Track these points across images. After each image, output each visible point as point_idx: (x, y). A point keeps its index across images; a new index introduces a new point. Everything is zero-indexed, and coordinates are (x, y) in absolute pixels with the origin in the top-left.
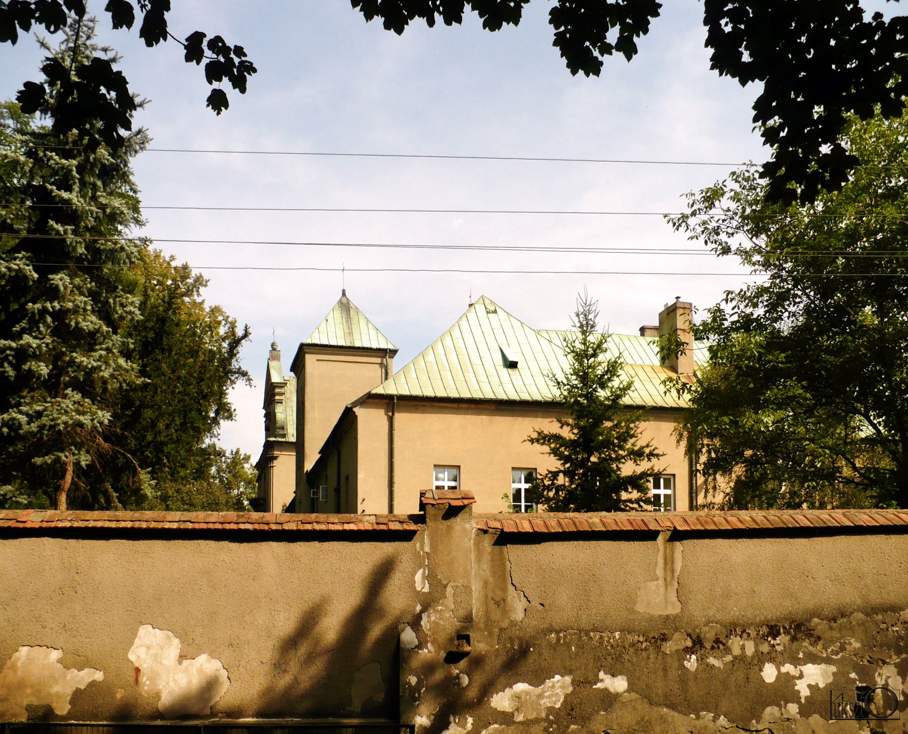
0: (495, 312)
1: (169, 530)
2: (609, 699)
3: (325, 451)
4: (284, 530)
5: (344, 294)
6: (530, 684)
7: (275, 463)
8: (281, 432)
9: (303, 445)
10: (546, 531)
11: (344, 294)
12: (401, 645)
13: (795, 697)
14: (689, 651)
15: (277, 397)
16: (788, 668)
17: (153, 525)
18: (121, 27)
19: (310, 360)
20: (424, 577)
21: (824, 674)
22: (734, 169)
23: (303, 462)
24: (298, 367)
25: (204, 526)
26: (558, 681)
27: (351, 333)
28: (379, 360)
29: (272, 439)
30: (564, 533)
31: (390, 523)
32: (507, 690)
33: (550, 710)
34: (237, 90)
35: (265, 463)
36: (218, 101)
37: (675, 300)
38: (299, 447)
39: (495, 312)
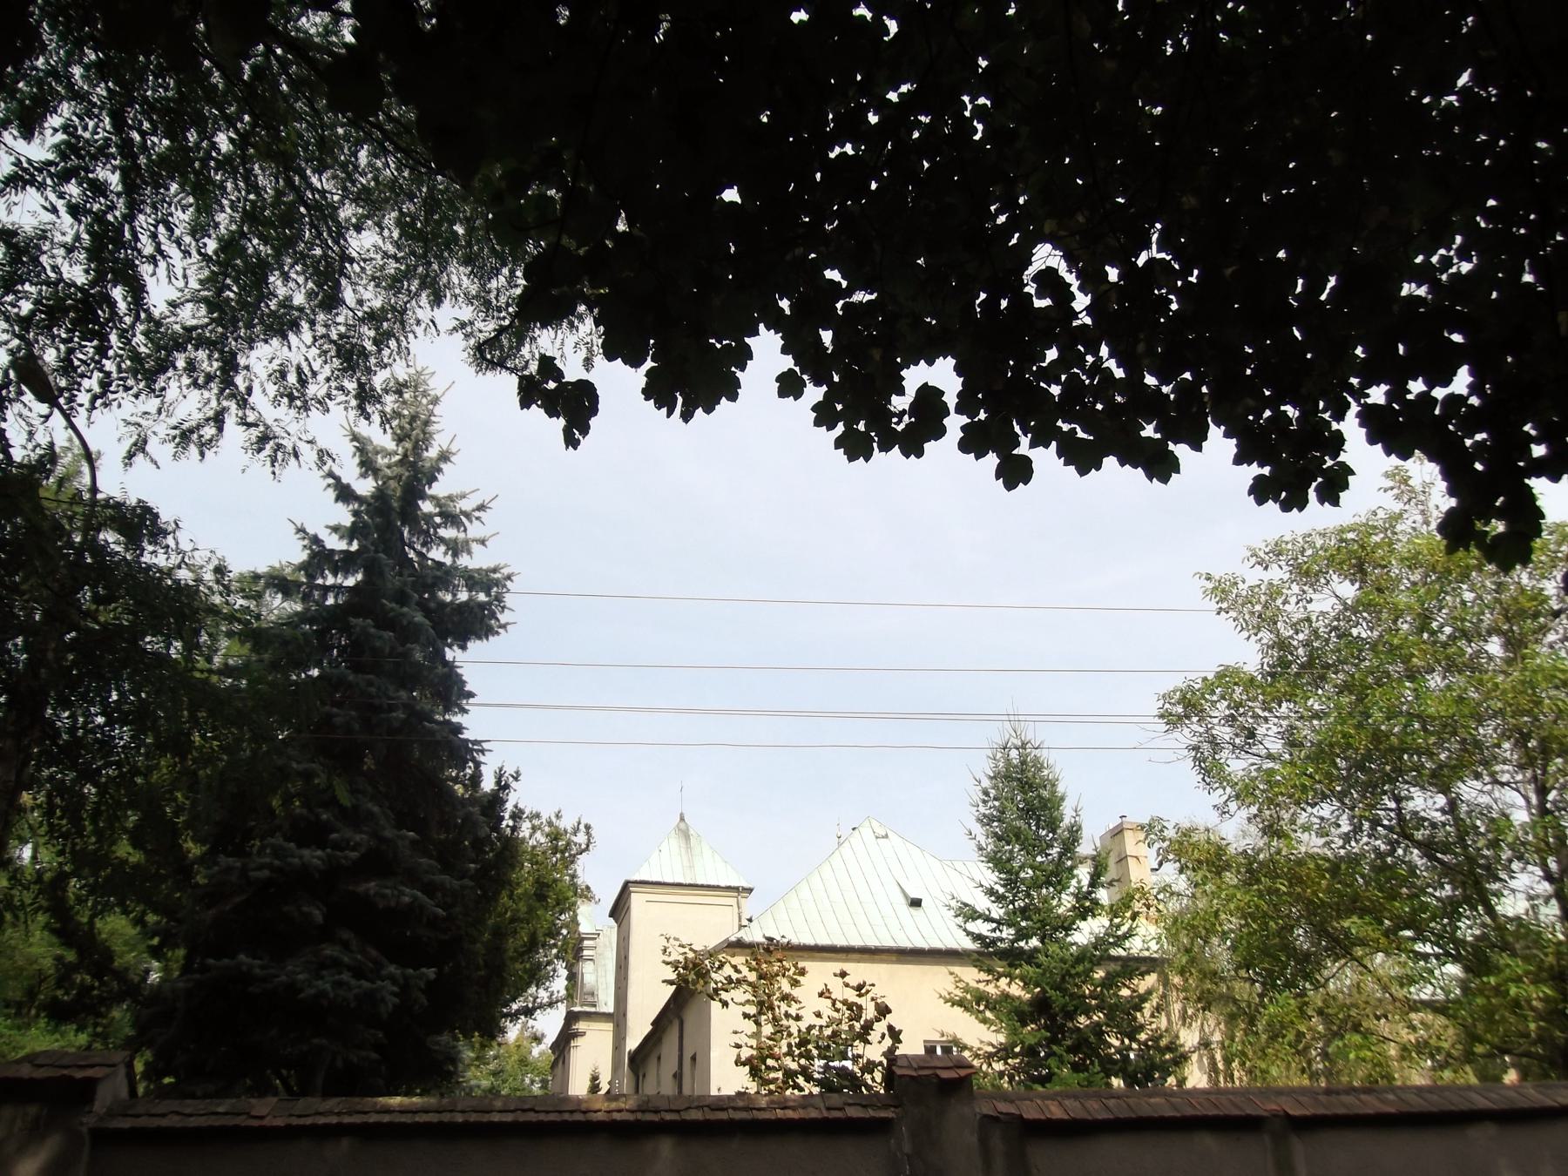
0: (886, 836)
1: (500, 1125)
3: (660, 1023)
4: (684, 1122)
5: (682, 819)
7: (579, 1041)
9: (625, 1015)
10: (1066, 1117)
11: (682, 819)
17: (473, 1118)
19: (637, 900)
22: (1203, 675)
23: (624, 1039)
24: (620, 910)
25: (552, 1117)
27: (691, 867)
28: (733, 901)
31: (847, 1108)
37: (1120, 821)
38: (618, 1018)
39: (886, 836)
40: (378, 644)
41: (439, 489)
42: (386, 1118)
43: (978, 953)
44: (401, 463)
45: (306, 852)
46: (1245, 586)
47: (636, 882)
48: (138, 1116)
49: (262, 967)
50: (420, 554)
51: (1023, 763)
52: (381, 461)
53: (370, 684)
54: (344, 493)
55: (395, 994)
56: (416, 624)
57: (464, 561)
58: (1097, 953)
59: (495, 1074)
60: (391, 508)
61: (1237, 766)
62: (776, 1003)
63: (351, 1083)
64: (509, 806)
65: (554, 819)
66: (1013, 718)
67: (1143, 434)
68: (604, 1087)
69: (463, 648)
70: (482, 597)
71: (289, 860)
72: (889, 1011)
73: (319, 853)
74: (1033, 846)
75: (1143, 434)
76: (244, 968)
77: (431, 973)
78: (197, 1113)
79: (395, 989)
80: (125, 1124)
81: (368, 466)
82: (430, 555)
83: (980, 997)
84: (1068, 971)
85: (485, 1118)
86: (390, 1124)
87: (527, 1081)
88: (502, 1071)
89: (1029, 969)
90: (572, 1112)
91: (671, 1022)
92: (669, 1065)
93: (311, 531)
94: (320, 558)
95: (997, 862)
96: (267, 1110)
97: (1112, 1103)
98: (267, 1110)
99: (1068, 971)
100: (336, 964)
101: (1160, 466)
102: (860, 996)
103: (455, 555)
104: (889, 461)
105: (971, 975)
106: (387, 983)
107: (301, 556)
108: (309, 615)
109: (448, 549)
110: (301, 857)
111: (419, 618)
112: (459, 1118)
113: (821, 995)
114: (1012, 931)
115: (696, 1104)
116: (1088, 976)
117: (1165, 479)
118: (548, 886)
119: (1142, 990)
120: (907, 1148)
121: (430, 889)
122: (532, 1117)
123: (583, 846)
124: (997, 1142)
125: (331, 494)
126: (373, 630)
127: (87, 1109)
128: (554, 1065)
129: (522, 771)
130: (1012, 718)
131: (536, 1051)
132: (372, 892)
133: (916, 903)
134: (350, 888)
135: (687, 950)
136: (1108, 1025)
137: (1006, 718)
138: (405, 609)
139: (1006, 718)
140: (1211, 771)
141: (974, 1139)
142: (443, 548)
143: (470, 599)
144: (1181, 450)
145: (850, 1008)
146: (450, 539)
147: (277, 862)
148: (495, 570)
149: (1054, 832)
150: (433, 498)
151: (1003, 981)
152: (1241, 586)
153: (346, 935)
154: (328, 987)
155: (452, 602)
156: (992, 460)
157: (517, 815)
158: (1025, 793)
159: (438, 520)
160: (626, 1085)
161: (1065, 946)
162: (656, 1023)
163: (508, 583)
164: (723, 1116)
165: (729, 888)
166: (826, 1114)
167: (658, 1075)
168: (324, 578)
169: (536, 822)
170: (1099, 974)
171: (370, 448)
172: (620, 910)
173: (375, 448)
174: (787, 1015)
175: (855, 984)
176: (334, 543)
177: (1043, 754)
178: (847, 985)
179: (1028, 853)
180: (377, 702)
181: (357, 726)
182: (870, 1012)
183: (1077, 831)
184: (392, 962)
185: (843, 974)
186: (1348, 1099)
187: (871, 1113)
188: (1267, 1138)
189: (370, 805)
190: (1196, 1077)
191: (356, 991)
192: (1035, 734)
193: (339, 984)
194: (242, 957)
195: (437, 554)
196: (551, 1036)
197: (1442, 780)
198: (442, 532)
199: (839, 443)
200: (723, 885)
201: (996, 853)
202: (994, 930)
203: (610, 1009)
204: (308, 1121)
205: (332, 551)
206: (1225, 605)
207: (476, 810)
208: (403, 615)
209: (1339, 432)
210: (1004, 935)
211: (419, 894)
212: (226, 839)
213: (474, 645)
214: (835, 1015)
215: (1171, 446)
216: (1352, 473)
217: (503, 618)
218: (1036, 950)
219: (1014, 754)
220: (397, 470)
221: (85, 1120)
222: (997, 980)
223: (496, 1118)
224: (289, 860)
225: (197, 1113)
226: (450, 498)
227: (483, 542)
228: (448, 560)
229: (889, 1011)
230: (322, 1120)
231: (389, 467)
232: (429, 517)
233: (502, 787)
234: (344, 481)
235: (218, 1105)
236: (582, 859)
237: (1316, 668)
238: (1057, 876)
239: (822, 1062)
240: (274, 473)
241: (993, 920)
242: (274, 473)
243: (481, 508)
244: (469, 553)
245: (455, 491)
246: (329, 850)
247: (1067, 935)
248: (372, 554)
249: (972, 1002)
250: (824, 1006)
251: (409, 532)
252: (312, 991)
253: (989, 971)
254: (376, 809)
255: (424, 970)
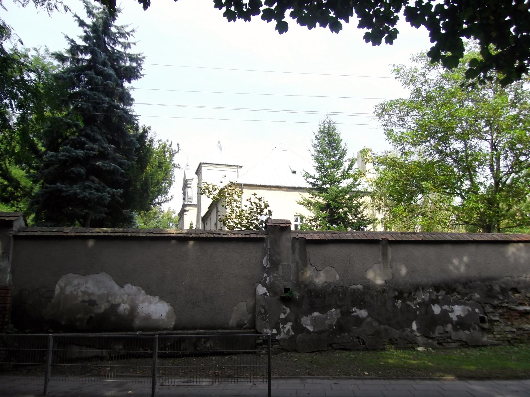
2: (359, 321)
3: (211, 208)
5: (219, 143)
6: (320, 313)
7: (186, 213)
8: (190, 200)
9: (200, 205)
11: (219, 143)
12: (257, 293)
13: (450, 321)
14: (397, 298)
15: (188, 185)
16: (446, 307)
17: (134, 235)
18: (117, 16)
19: (204, 169)
20: (267, 259)
21: (463, 311)
23: (200, 212)
24: (198, 172)
26: (334, 312)
29: (186, 203)
30: (335, 240)
32: (309, 316)
33: (331, 326)
34: (430, 38)
35: (182, 213)
36: (149, 128)
38: (198, 206)
40: (96, 81)
41: (117, 23)
42: (106, 234)
43: (311, 189)
44: (102, 12)
45: (77, 151)
46: (406, 69)
47: (203, 163)
48: (27, 232)
49: (66, 188)
50: (112, 48)
51: (329, 127)
52: (95, 11)
53: (95, 95)
54: (82, 23)
55: (110, 197)
56: (109, 74)
57: (128, 51)
58: (346, 191)
59: (157, 222)
60: (98, 30)
61: (397, 130)
62: (233, 202)
63: (100, 224)
64: (149, 138)
65: (166, 142)
66: (327, 113)
67: (331, 15)
68: (194, 227)
69: (130, 82)
70: (134, 65)
71: (72, 153)
72: (268, 206)
73: (82, 151)
74: (328, 155)
75: (331, 15)
76: (59, 188)
77: (121, 191)
78: (55, 231)
79: (110, 196)
80: (24, 234)
81: (90, 13)
82: (116, 48)
83: (309, 202)
84: (337, 195)
85: (138, 235)
86: (107, 236)
87: (171, 225)
88: (160, 221)
89: (324, 194)
90: (165, 234)
91: (214, 208)
92: (214, 221)
93: (71, 37)
94: (75, 49)
95: (317, 159)
96: (68, 231)
97: (334, 235)
98: (68, 231)
99: (337, 195)
100: (90, 187)
101: (336, 27)
102: (260, 201)
103: (125, 48)
104: (240, 21)
105: (307, 195)
106: (106, 193)
107: (68, 47)
108: (72, 69)
109: (122, 46)
110: (76, 153)
111: (111, 72)
112: (129, 235)
113: (247, 200)
114: (321, 182)
115: (204, 232)
116: (344, 197)
117: (337, 32)
118: (162, 163)
119: (360, 202)
120: (269, 247)
121: (121, 164)
122: (152, 235)
123: (177, 151)
124: (297, 245)
125: (77, 24)
126: (94, 76)
127: (11, 229)
128: (179, 220)
129: (151, 126)
130: (327, 113)
131: (174, 216)
132: (100, 165)
133: (294, 172)
134: (94, 163)
135: (205, 184)
136: (349, 212)
137: (325, 113)
138: (106, 68)
139: (325, 113)
140: (389, 133)
141: (290, 244)
142: (120, 46)
143: (130, 65)
144: (342, 21)
145: (256, 204)
146: (123, 43)
147: (68, 154)
148: (139, 55)
149: (337, 150)
150: (116, 27)
151: (317, 197)
152: (404, 68)
153: (93, 178)
154: (87, 194)
155: (124, 66)
156: (274, 22)
157: (151, 141)
158: (329, 137)
159: (117, 35)
160: (201, 227)
161: (338, 188)
162: (209, 208)
163: (144, 59)
164: (212, 236)
165: (234, 166)
166: (244, 236)
167: (211, 224)
168: (78, 55)
169: (160, 143)
170: (348, 196)
171: (90, 6)
172: (198, 172)
173: (92, 6)
174: (236, 206)
175: (258, 197)
176: (81, 43)
177: (336, 126)
178: (256, 198)
179: (328, 157)
180: (98, 101)
181: (91, 109)
182: (263, 207)
183: (345, 151)
184: (109, 187)
185: (255, 194)
186: (406, 235)
187: (258, 236)
188: (380, 247)
189: (98, 136)
190: (380, 229)
191: (96, 196)
192: (333, 118)
193: (91, 193)
194: (58, 184)
195: (118, 48)
196: (178, 211)
197: (463, 137)
198: (119, 39)
199: (225, 15)
200: (232, 165)
201: (317, 156)
202: (315, 182)
203: (196, 203)
204: (82, 234)
205: (79, 46)
206: (397, 76)
207: (134, 139)
208: (105, 70)
209: (397, 16)
210: (318, 183)
211: (116, 166)
212: (52, 146)
213: (133, 81)
214: (252, 207)
215: (339, 20)
216: (398, 33)
217: (142, 72)
218: (328, 188)
219: (326, 125)
220: (101, 15)
221: (11, 233)
222: (315, 197)
223: (141, 235)
224: (72, 153)
225: (55, 231)
226: (122, 27)
227: (135, 44)
228: (122, 50)
229: (268, 206)
230: (86, 234)
231: (98, 14)
232: (115, 34)
233: (145, 131)
234: (81, 19)
235: (53, 229)
236: (176, 155)
237: (429, 99)
238: (337, 165)
239: (246, 221)
240: (49, 14)
241: (315, 178)
242: (49, 14)
243: (133, 31)
244: (130, 48)
245: (124, 24)
246: (85, 151)
247: (339, 184)
248: (92, 47)
249: (308, 204)
250: (248, 204)
251: (108, 39)
252: (82, 195)
253: (313, 194)
254: (100, 137)
255: (119, 190)
